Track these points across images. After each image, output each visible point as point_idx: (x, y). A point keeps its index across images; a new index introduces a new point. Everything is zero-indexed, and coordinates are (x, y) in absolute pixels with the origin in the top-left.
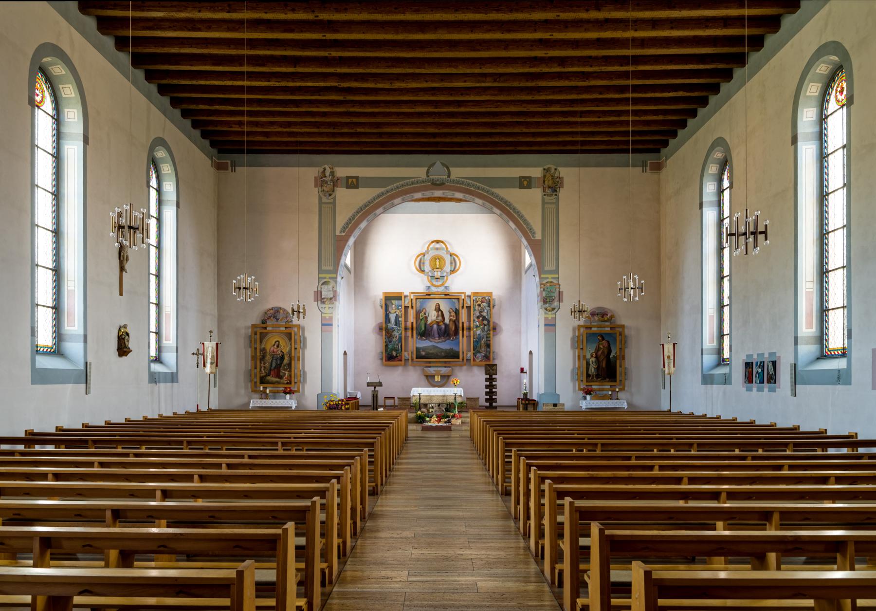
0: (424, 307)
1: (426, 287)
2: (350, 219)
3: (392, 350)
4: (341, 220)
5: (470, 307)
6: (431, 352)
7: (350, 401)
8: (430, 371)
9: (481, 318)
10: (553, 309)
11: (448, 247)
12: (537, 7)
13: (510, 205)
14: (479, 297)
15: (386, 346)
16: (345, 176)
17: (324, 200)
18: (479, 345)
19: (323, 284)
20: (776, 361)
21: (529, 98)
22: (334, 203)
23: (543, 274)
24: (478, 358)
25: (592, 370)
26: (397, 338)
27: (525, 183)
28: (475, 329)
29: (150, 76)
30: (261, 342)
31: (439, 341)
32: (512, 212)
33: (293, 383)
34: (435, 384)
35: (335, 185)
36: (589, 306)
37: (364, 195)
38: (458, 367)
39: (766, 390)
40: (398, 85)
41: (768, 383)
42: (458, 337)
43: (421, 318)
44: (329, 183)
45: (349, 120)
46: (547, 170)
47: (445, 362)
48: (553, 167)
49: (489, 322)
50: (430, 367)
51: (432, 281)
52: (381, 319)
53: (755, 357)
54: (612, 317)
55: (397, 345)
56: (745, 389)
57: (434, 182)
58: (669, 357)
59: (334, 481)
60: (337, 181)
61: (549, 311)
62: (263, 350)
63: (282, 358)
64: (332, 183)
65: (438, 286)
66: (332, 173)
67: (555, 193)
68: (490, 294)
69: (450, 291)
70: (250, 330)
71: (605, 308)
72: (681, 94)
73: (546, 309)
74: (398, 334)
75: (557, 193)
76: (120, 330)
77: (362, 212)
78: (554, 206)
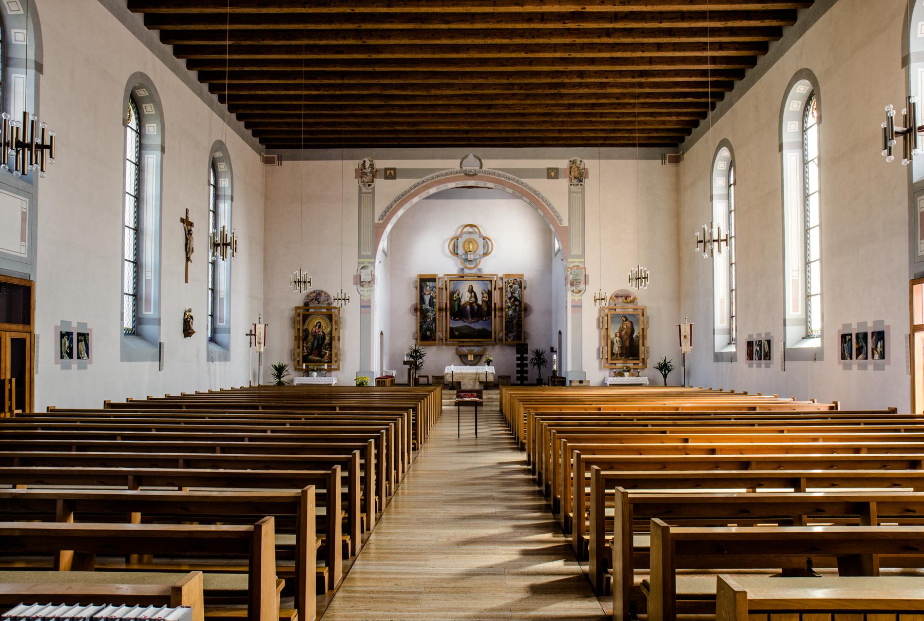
2: (388, 208)
3: (427, 330)
4: (379, 209)
5: (502, 288)
6: (464, 332)
7: (387, 378)
9: (513, 299)
10: (580, 291)
11: (481, 230)
12: (555, 33)
13: (539, 194)
14: (510, 279)
15: (421, 326)
16: (384, 168)
17: (364, 190)
19: (361, 269)
20: (770, 340)
21: (553, 102)
22: (373, 193)
23: (570, 258)
24: (510, 338)
25: (616, 349)
27: (553, 174)
28: (507, 310)
29: (179, 52)
30: (304, 323)
32: (541, 201)
33: (333, 361)
34: (469, 363)
35: (374, 176)
36: (609, 293)
37: (401, 185)
39: (855, 367)
40: (433, 92)
41: (764, 359)
43: (455, 299)
44: (368, 174)
45: (388, 120)
46: (573, 162)
47: (478, 342)
48: (579, 160)
49: (520, 302)
50: (463, 346)
51: (465, 263)
53: (755, 336)
54: (635, 299)
55: (432, 325)
56: (747, 365)
57: (467, 173)
58: (685, 337)
60: (376, 172)
61: (576, 293)
63: (324, 338)
64: (371, 175)
65: (470, 269)
66: (372, 166)
67: (581, 183)
68: (522, 276)
69: (483, 273)
70: (294, 312)
71: (629, 291)
72: (689, 100)
73: (573, 291)
75: (583, 183)
76: (185, 314)
78: (580, 195)
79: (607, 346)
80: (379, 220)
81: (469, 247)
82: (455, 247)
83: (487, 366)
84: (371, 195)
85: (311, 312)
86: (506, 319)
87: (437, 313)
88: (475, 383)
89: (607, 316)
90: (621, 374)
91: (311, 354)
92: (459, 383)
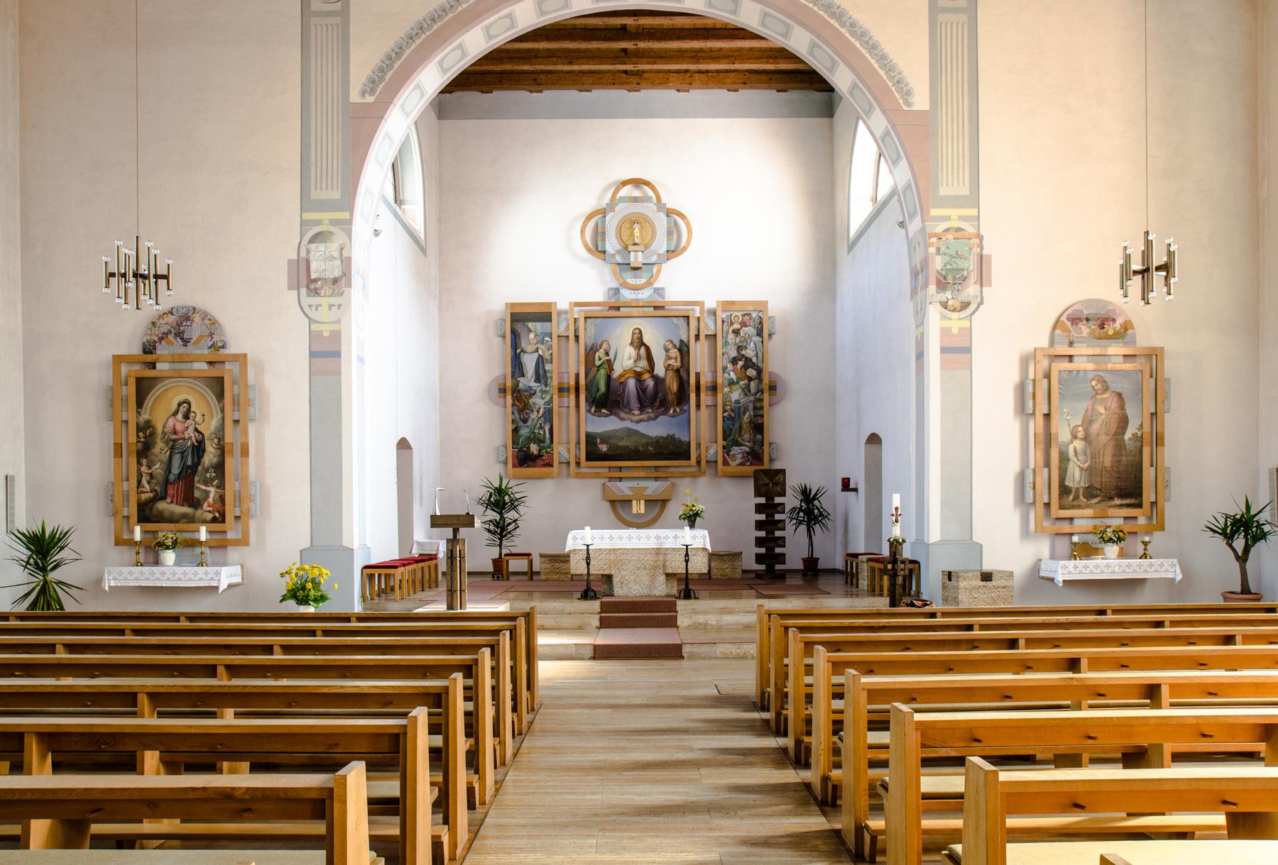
0: (603, 338)
1: (610, 289)
4: (363, 61)
5: (715, 335)
8: (621, 491)
9: (741, 363)
10: (965, 305)
15: (516, 431)
18: (737, 426)
19: (312, 240)
25: (1076, 477)
26: (541, 411)
28: (726, 389)
30: (140, 404)
31: (642, 417)
32: (847, 35)
33: (229, 517)
38: (687, 481)
42: (685, 408)
43: (598, 363)
50: (620, 479)
51: (624, 275)
52: (499, 367)
54: (1127, 326)
55: (541, 427)
59: (459, 676)
61: (954, 310)
62: (146, 429)
63: (199, 449)
65: (636, 288)
73: (945, 305)
74: (543, 402)
77: (424, 37)
78: (963, 18)
79: (1047, 464)
80: (363, 94)
81: (632, 235)
82: (599, 234)
83: (687, 528)
84: (338, 20)
85: (161, 371)
86: (724, 411)
87: (555, 397)
88: (653, 577)
89: (1048, 376)
90: (1085, 551)
91: (163, 498)
92: (608, 578)
